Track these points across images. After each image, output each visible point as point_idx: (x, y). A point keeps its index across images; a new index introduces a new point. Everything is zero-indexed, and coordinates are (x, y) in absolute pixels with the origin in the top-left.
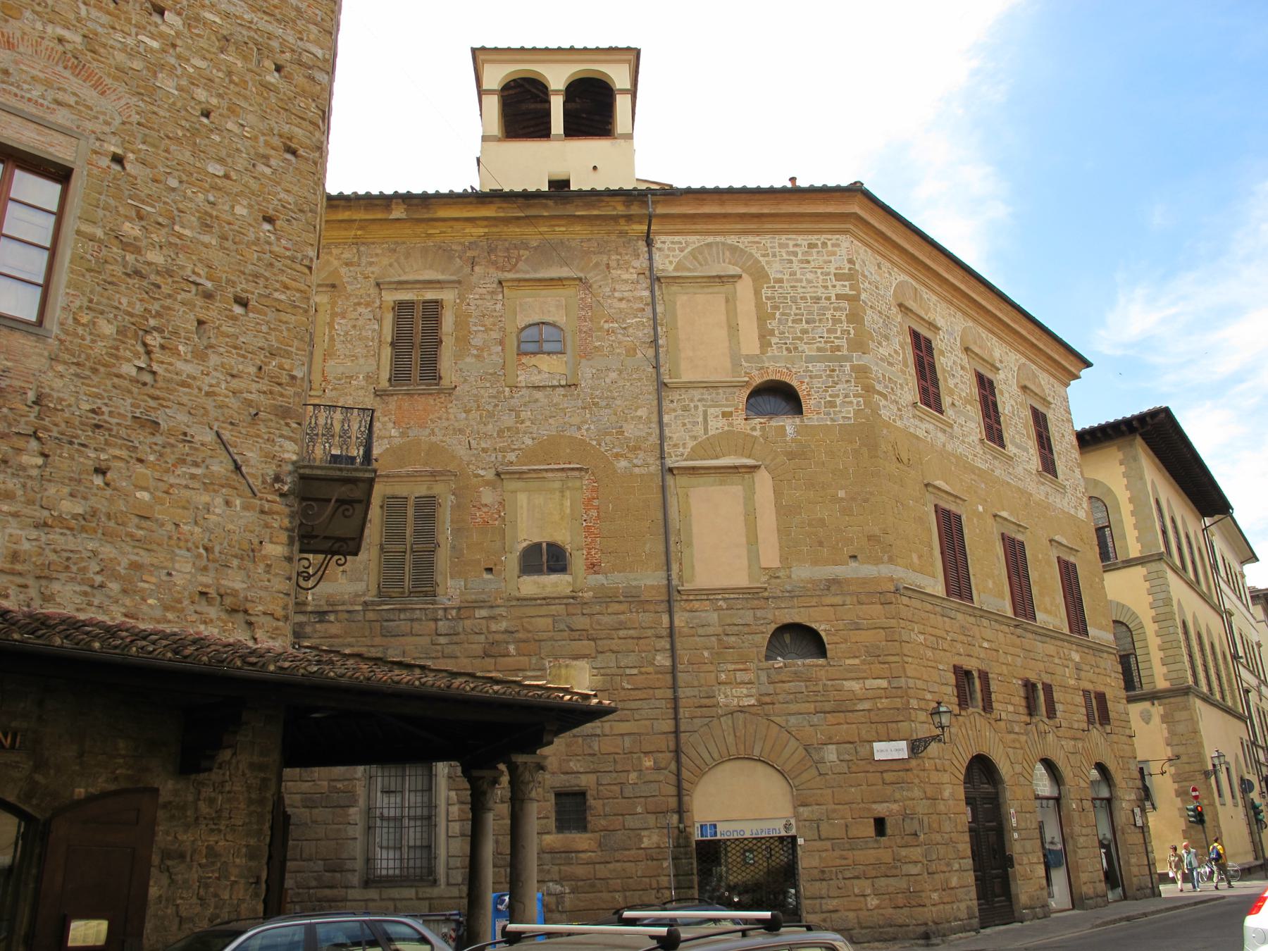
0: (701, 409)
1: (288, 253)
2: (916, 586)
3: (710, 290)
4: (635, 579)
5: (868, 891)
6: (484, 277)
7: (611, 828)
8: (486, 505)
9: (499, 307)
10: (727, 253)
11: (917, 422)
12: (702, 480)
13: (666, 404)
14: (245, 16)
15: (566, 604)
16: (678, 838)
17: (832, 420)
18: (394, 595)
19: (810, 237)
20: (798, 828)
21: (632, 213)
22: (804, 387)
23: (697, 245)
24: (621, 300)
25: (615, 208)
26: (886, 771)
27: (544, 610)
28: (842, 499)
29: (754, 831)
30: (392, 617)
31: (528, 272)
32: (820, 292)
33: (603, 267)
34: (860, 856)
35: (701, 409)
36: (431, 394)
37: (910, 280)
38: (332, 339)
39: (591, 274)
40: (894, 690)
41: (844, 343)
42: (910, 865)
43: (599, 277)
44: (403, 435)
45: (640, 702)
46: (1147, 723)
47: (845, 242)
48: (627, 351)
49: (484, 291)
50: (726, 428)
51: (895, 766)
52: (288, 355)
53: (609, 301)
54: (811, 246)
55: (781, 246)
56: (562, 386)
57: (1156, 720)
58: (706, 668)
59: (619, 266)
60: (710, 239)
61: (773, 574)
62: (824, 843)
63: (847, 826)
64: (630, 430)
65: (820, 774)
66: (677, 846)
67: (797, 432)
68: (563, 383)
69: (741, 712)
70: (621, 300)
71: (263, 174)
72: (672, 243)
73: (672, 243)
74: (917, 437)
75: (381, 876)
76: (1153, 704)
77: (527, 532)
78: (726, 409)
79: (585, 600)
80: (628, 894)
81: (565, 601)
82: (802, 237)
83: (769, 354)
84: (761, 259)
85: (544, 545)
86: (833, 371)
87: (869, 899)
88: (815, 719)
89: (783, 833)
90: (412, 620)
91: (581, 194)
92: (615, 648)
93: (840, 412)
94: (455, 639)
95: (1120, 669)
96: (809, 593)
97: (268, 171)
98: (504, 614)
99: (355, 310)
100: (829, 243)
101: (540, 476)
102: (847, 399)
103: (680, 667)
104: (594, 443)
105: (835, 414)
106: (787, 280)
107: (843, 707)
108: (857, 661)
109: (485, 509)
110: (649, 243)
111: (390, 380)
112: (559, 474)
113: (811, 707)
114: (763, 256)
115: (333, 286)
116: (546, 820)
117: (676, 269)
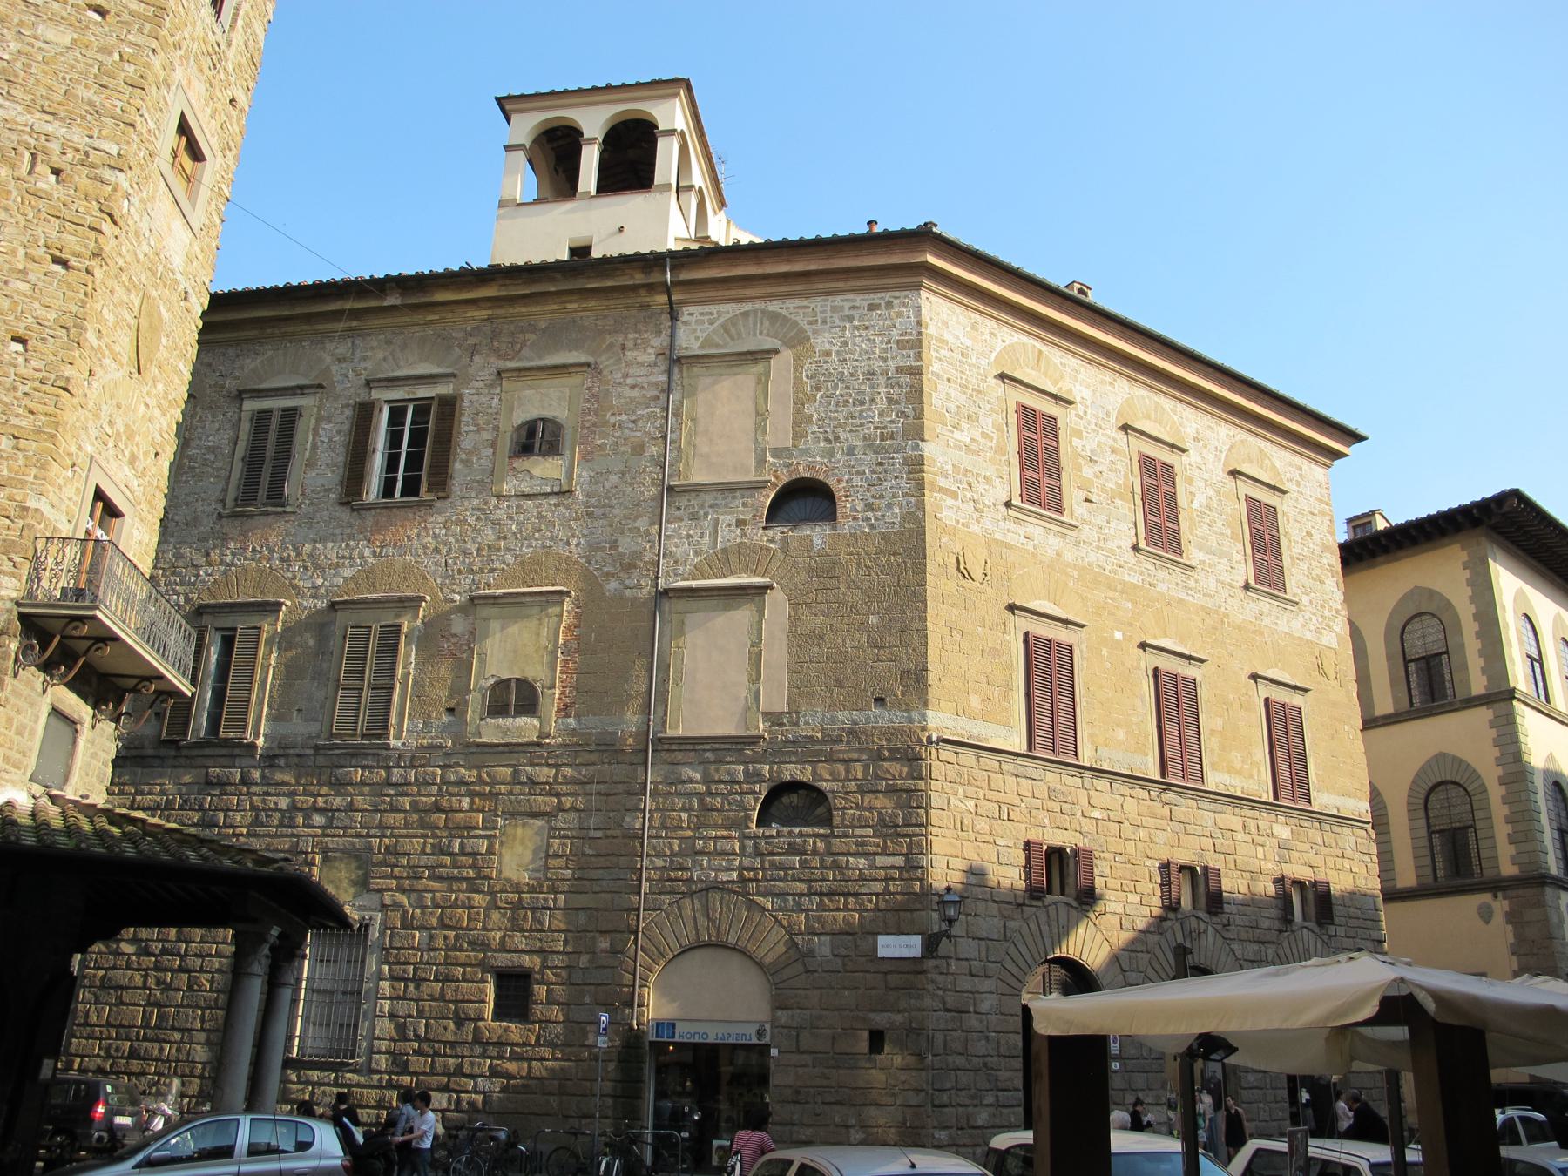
1: (38, 375)
5: (852, 1121)
6: (483, 366)
8: (456, 635)
9: (496, 402)
10: (767, 323)
11: (1011, 526)
12: (702, 603)
14: (18, 119)
19: (872, 296)
20: (773, 1037)
21: (651, 281)
23: (732, 315)
24: (633, 387)
25: (632, 277)
26: (890, 972)
30: (343, 763)
31: (532, 360)
33: (618, 348)
38: (314, 447)
39: (603, 358)
43: (611, 361)
45: (601, 871)
46: (1487, 922)
48: (633, 449)
49: (481, 384)
52: (22, 484)
53: (619, 389)
54: (872, 307)
55: (834, 309)
56: (556, 494)
57: (1499, 919)
60: (748, 307)
62: (805, 1056)
63: (834, 1038)
65: (808, 971)
68: (556, 489)
70: (633, 387)
71: (17, 291)
72: (702, 314)
73: (702, 314)
74: (1008, 546)
76: (1496, 897)
80: (564, 1098)
82: (861, 296)
84: (807, 327)
87: (852, 1131)
89: (755, 1041)
91: (605, 260)
95: (1374, 849)
97: (24, 287)
100: (896, 302)
105: (876, 519)
109: (454, 640)
110: (674, 317)
111: (236, 500)
112: (538, 598)
114: (810, 323)
117: (702, 347)
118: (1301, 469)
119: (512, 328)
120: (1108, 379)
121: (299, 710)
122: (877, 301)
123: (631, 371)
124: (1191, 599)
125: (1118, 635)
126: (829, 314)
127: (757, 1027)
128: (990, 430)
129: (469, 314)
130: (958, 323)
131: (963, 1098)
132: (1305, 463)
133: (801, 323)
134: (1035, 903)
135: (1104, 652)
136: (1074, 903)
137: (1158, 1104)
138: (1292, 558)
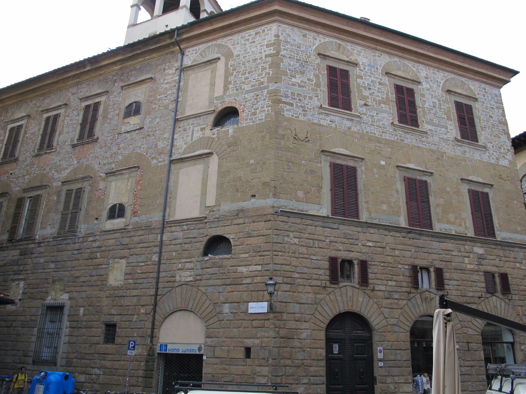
0: (192, 128)
2: (298, 210)
3: (205, 69)
4: (151, 218)
7: (123, 343)
8: (100, 189)
10: (216, 49)
13: (177, 129)
15: (122, 232)
16: (149, 351)
17: (253, 122)
18: (62, 233)
19: (257, 29)
22: (241, 108)
23: (204, 48)
24: (167, 83)
26: (255, 320)
27: (112, 236)
28: (252, 164)
29: (184, 350)
30: (61, 243)
32: (258, 56)
33: (163, 70)
34: (233, 369)
35: (192, 128)
36: (90, 143)
37: (331, 39)
39: (157, 75)
40: (265, 272)
41: (265, 80)
42: (261, 378)
43: (160, 75)
44: (78, 162)
47: (274, 27)
50: (201, 136)
51: (260, 317)
54: (256, 34)
55: (242, 38)
58: (173, 261)
59: (169, 68)
60: (210, 44)
61: (211, 209)
64: (160, 145)
66: (149, 355)
67: (234, 132)
69: (186, 284)
70: (167, 83)
72: (193, 51)
74: (320, 125)
75: (44, 360)
77: (112, 200)
78: (203, 126)
79: (129, 230)
81: (121, 231)
83: (228, 94)
84: (231, 47)
85: (118, 205)
86: (258, 95)
88: (221, 289)
89: (197, 353)
90: (67, 244)
92: (137, 253)
93: (258, 117)
94: (80, 251)
96: (227, 218)
98: (98, 239)
99: (72, 113)
100: (266, 30)
101: (121, 173)
102: (263, 109)
103: (162, 262)
104: (145, 154)
106: (242, 54)
107: (236, 283)
108: (246, 255)
109: (100, 191)
112: (128, 171)
113: (219, 282)
114: (232, 45)
115: (66, 105)
116: (98, 338)
118: (485, 89)
119: (128, 70)
120: (377, 54)
121: (50, 224)
122: (259, 31)
123: (166, 78)
124: (424, 146)
125: (383, 163)
126: (240, 40)
127: (198, 346)
128: (312, 77)
129: (114, 68)
130: (296, 34)
131: (290, 380)
132: (488, 87)
133: (229, 46)
134: (333, 286)
135: (375, 170)
136: (357, 286)
137: (406, 383)
138: (481, 127)
